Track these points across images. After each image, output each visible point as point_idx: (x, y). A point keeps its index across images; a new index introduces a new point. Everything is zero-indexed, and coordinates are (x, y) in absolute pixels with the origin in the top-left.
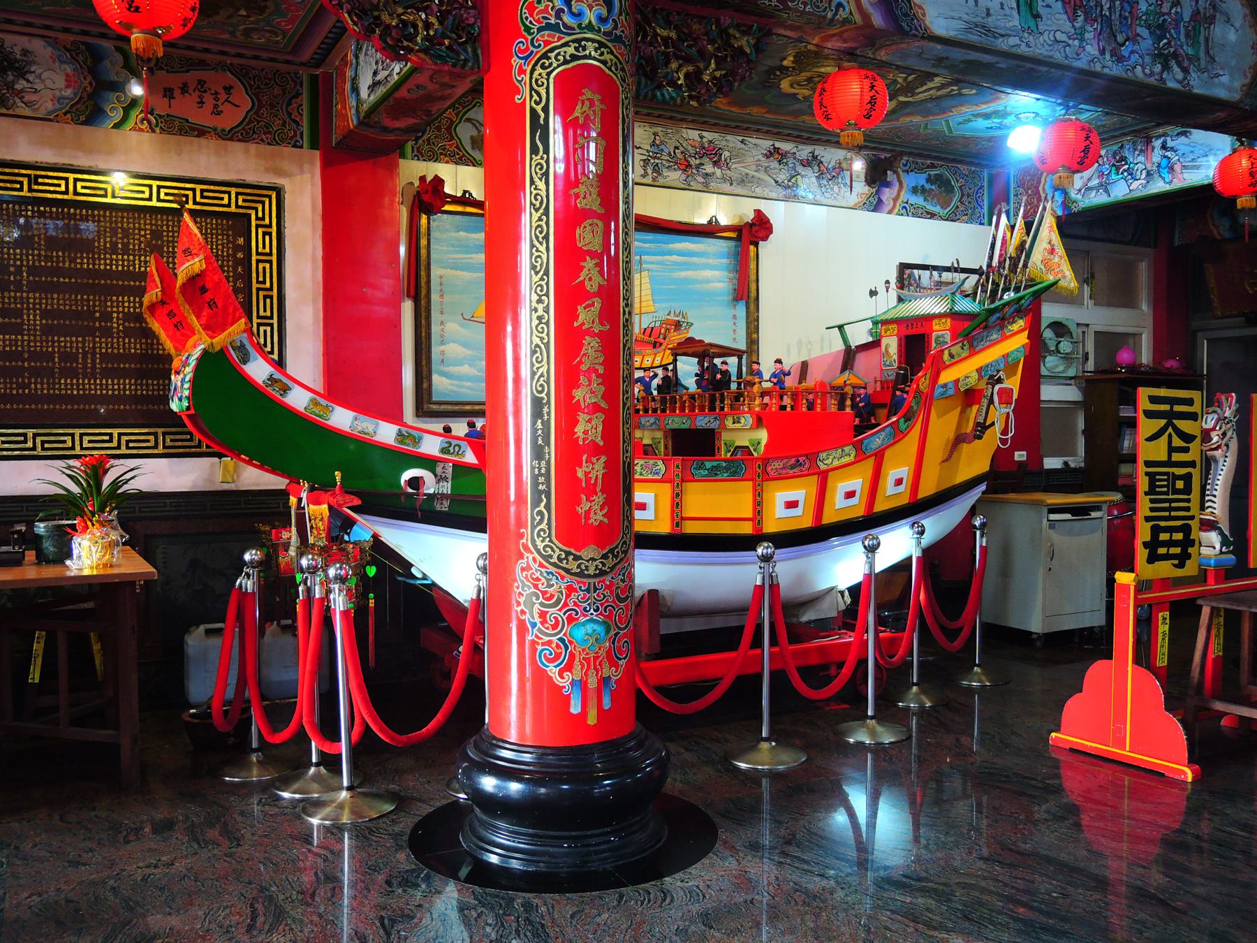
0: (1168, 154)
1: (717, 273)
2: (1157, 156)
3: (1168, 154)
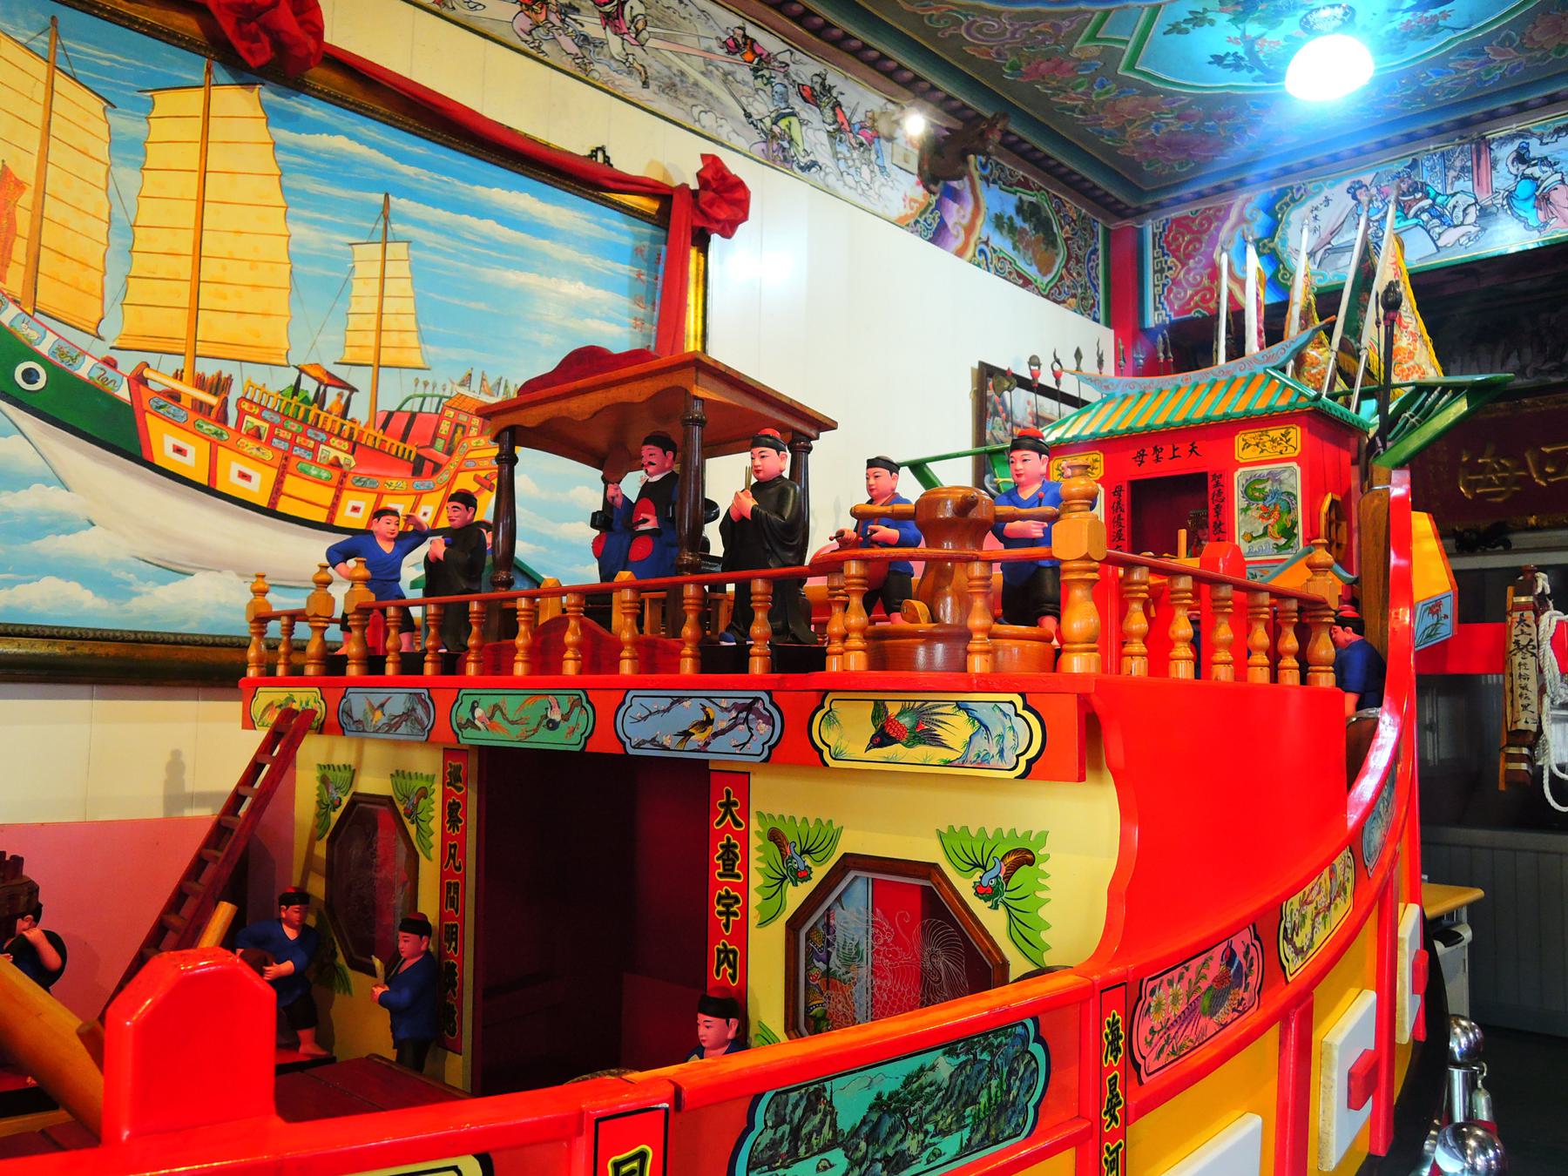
0: (1536, 171)
1: (600, 294)
2: (1504, 175)
3: (1536, 171)
